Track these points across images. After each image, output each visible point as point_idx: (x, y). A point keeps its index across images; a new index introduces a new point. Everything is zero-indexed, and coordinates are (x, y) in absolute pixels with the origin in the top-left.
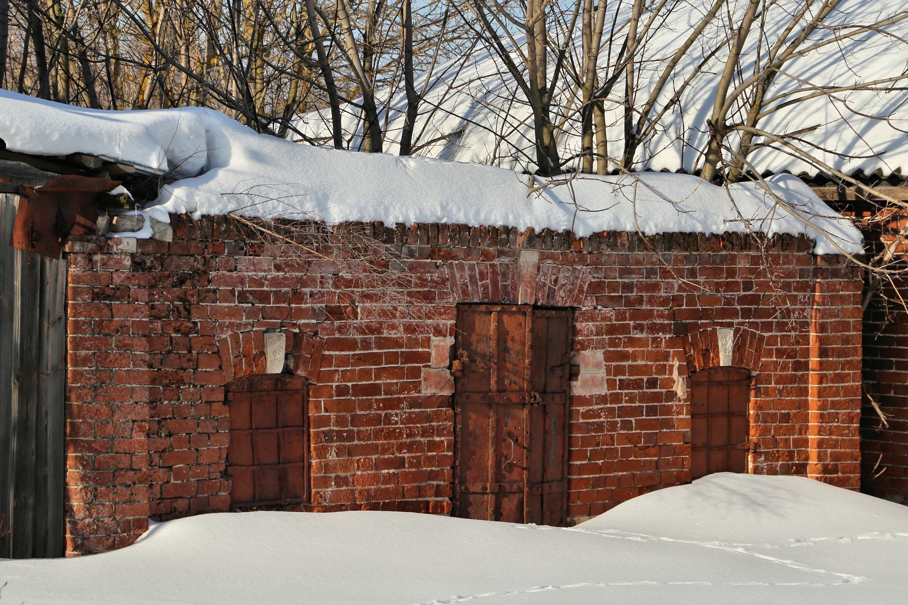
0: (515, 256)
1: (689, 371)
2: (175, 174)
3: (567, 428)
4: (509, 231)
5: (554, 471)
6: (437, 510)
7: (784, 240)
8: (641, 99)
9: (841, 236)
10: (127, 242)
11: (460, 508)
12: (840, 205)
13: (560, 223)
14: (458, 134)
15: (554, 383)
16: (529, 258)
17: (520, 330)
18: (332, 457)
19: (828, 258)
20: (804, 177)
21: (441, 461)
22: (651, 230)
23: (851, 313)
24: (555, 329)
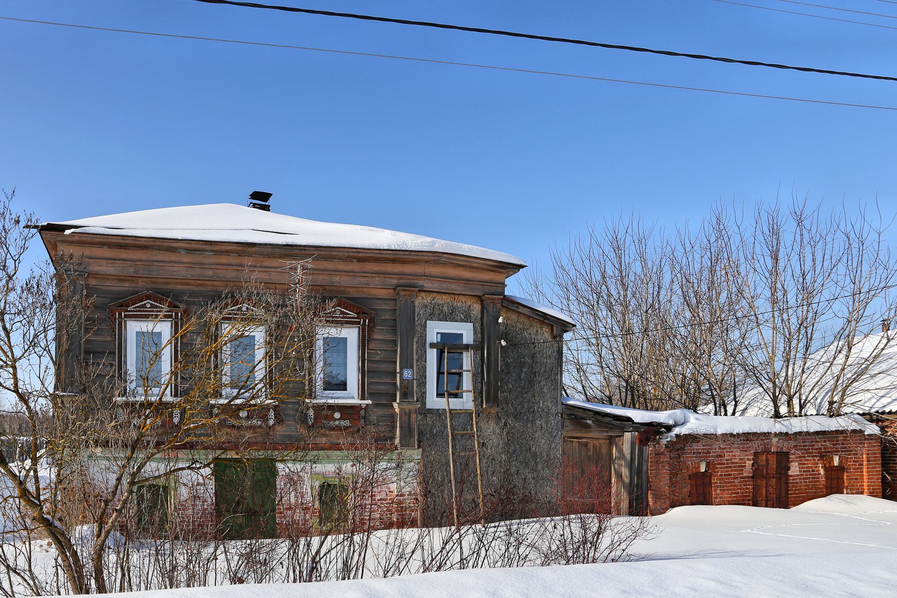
0: (771, 439)
1: (825, 467)
2: (676, 425)
3: (787, 483)
4: (769, 433)
5: (783, 494)
6: (749, 505)
7: (854, 431)
8: (804, 397)
9: (872, 429)
10: (664, 442)
11: (755, 504)
12: (871, 421)
13: (784, 430)
14: (746, 409)
15: (783, 472)
16: (775, 440)
17: (773, 460)
18: (718, 492)
19: (868, 435)
20: (858, 414)
21: (750, 492)
22: (812, 430)
23: (877, 450)
24: (783, 458)
